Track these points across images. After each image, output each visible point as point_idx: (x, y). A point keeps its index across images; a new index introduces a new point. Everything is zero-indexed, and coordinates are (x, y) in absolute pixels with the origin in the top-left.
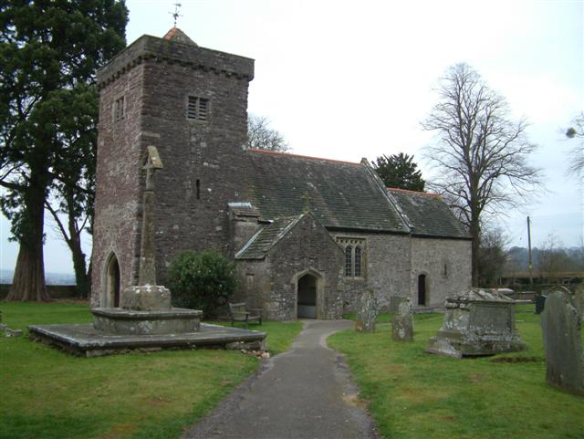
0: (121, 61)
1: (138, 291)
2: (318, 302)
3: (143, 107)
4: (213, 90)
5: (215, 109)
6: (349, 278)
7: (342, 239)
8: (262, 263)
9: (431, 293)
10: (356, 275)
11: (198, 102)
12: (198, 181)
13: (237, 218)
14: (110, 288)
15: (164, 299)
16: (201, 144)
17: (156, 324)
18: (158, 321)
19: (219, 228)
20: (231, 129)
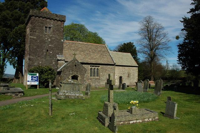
19: (54, 63)
20: (58, 36)
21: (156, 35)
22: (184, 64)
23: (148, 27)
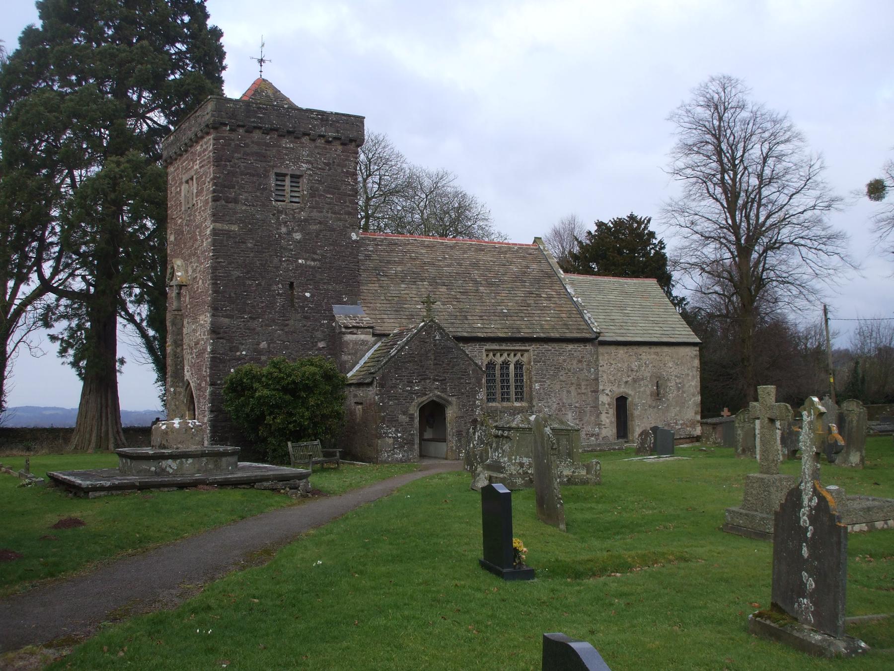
2: (449, 437)
3: (214, 191)
4: (308, 162)
6: (505, 404)
7: (495, 352)
8: (371, 388)
10: (516, 400)
11: (288, 179)
12: (292, 284)
13: (343, 330)
17: (182, 463)
18: (184, 460)
19: (321, 345)
20: (335, 213)
21: (690, 111)
23: (717, 134)
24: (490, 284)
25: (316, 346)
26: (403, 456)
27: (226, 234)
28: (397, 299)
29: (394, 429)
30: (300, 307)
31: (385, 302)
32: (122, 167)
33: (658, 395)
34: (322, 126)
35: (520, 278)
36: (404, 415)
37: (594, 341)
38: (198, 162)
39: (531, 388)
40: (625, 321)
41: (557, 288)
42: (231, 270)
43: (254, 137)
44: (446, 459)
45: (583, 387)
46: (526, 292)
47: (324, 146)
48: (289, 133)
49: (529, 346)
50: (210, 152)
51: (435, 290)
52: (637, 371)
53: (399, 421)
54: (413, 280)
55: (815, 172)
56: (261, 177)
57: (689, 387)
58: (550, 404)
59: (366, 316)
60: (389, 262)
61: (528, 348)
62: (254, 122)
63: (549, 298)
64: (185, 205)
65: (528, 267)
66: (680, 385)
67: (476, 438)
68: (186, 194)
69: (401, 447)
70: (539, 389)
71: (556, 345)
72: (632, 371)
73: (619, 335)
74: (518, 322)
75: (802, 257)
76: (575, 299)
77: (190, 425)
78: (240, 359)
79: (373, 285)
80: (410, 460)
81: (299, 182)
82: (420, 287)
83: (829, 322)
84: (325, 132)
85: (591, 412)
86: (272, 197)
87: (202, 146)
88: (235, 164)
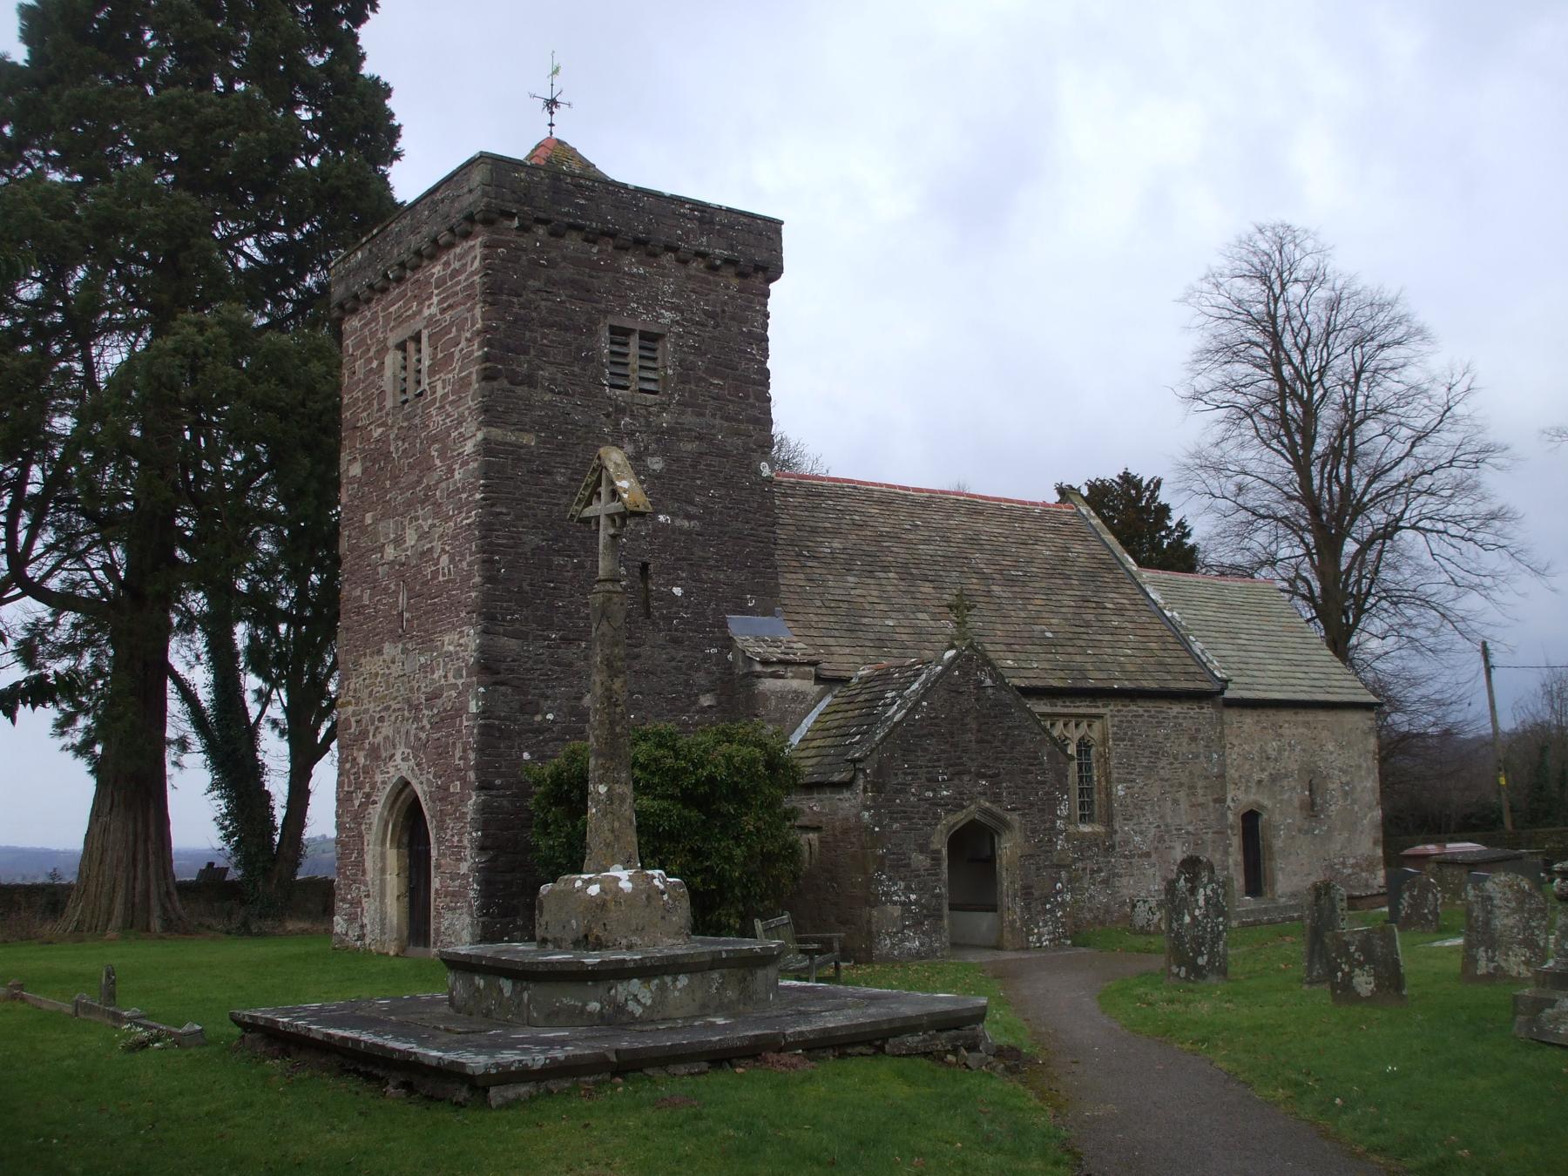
0: (403, 242)
1: (594, 890)
2: (1007, 901)
3: (486, 358)
4: (674, 308)
5: (681, 362)
8: (846, 794)
9: (1279, 863)
10: (1083, 817)
11: (634, 341)
12: (645, 567)
13: (758, 668)
14: (393, 884)
15: (667, 910)
16: (649, 460)
17: (663, 988)
18: (668, 979)
19: (706, 701)
20: (727, 418)
22: (143, 319)
24: (1010, 581)
25: (695, 703)
26: (922, 945)
27: (512, 453)
28: (845, 605)
29: (902, 884)
30: (663, 617)
31: (824, 611)
32: (208, 334)
33: (1312, 808)
34: (702, 234)
35: (1059, 568)
36: (921, 852)
37: (1210, 696)
38: (435, 300)
39: (1109, 794)
40: (1244, 659)
41: (1129, 591)
42: (521, 532)
43: (567, 248)
44: (998, 947)
45: (1200, 792)
46: (1076, 598)
47: (703, 275)
48: (639, 242)
49: (1105, 706)
50: (473, 274)
51: (912, 589)
52: (1276, 760)
53: (913, 867)
54: (868, 568)
55: (1457, 399)
56: (581, 334)
57: (1363, 791)
58: (1143, 827)
59: (795, 639)
60: (814, 531)
61: (1101, 711)
62: (567, 214)
63: (1120, 611)
64: (394, 396)
65: (1067, 549)
66: (1347, 788)
67: (1201, 903)
68: (398, 372)
69: (918, 924)
70: (1125, 797)
71: (1151, 705)
72: (1268, 758)
73: (1242, 686)
74: (1078, 658)
75: (1433, 555)
76: (1168, 614)
77: (656, 882)
78: (539, 730)
79: (794, 576)
80: (934, 952)
81: (654, 350)
82: (884, 582)
83: (1495, 674)
84: (708, 246)
85: (1214, 842)
86: (603, 375)
87: (447, 264)
88: (530, 302)
